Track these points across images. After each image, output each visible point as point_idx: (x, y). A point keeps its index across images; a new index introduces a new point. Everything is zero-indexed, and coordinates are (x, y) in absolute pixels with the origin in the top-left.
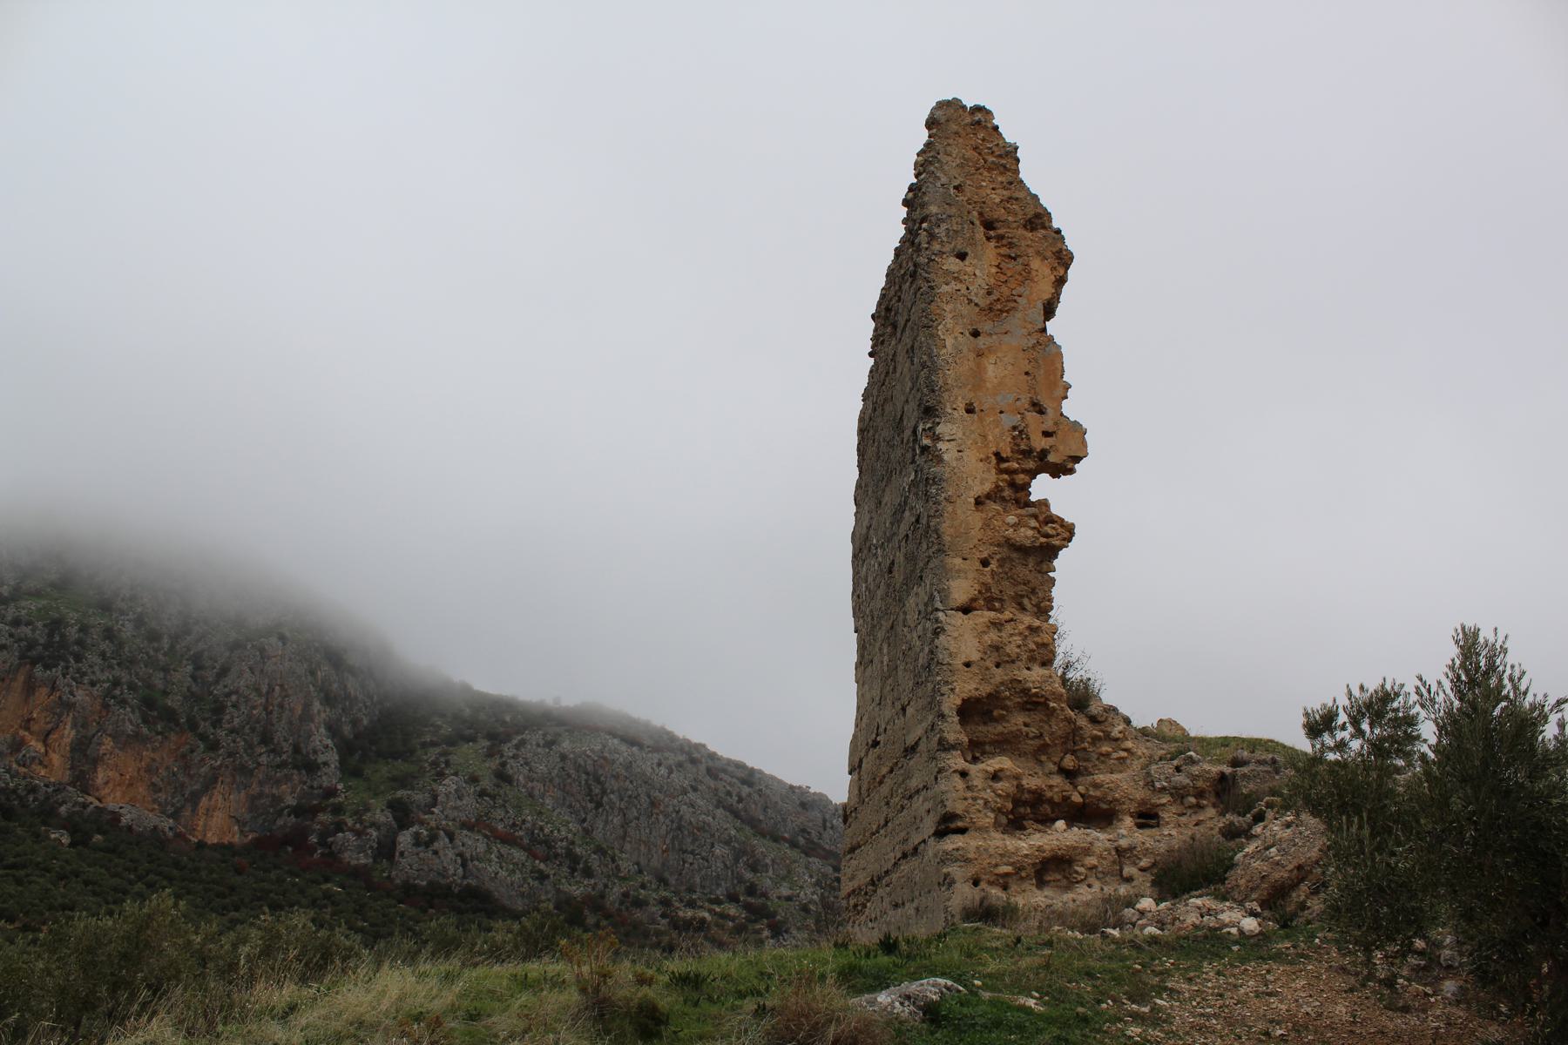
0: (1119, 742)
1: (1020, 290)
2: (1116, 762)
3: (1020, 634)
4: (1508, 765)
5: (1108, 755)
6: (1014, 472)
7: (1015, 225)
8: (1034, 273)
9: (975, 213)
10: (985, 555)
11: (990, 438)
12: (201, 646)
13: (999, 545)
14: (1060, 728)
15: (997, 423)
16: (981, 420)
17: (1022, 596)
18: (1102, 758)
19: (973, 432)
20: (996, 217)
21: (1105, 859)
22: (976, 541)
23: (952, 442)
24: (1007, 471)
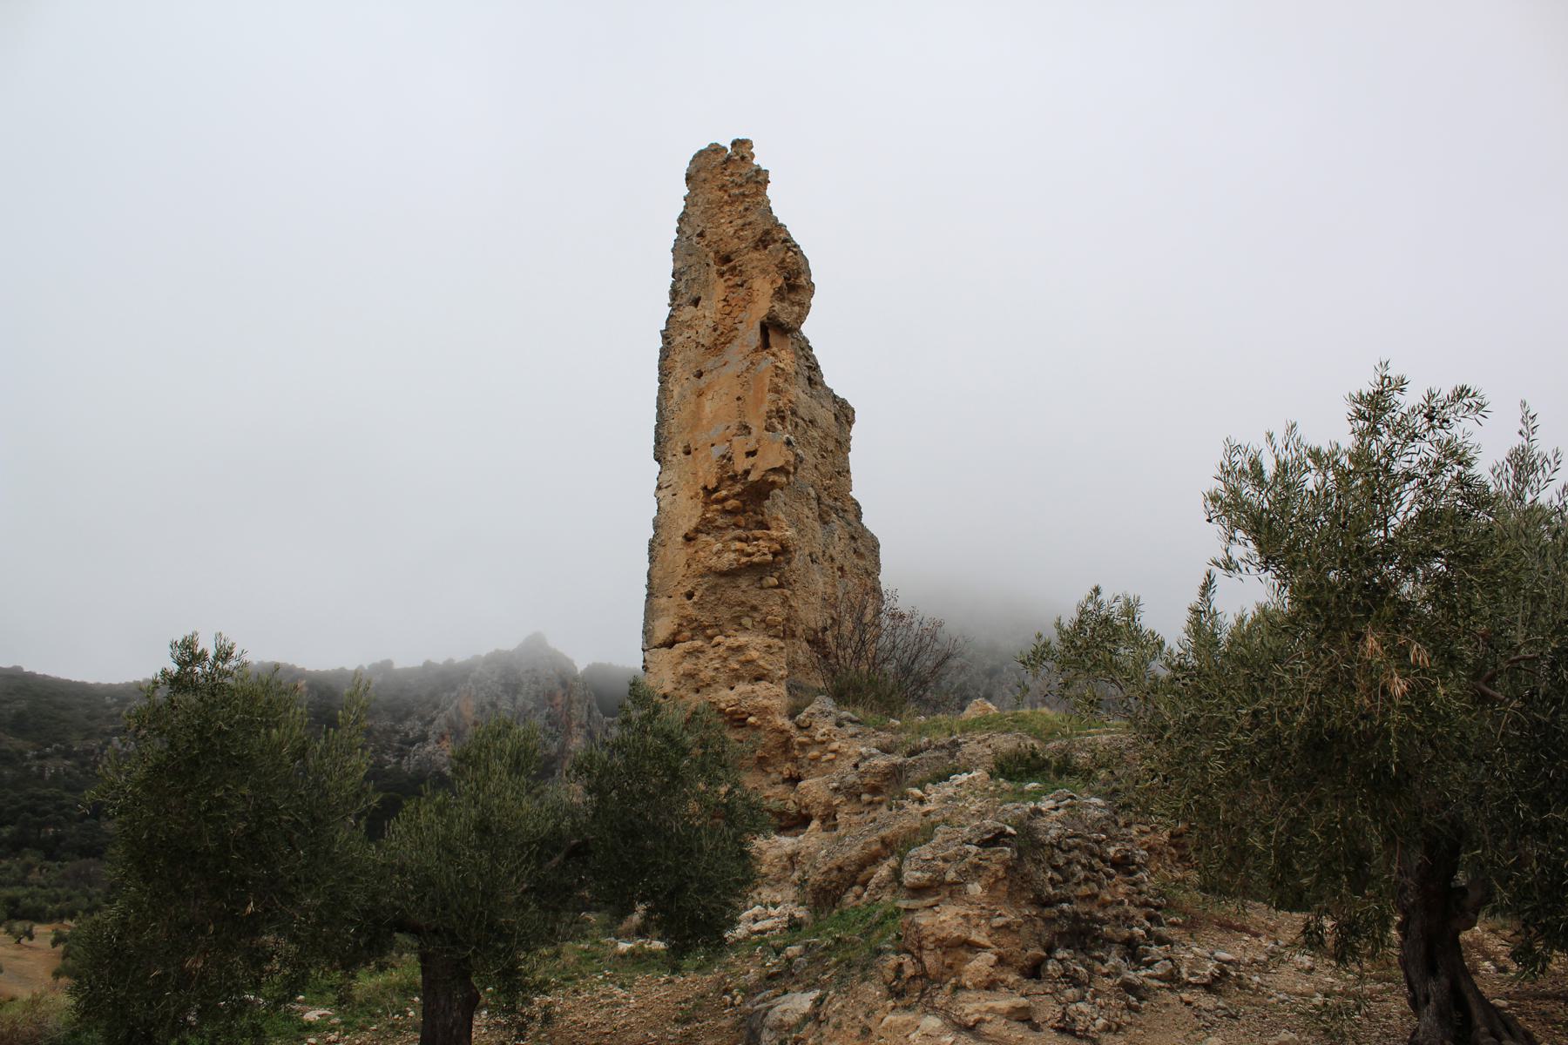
1: (742, 315)
2: (827, 765)
3: (720, 656)
4: (39, 833)
5: (816, 759)
6: (725, 499)
7: (745, 251)
8: (755, 294)
9: (712, 254)
10: (689, 588)
11: (701, 474)
12: (963, 678)
13: (702, 576)
14: (770, 740)
15: (708, 457)
16: (695, 458)
17: (739, 617)
18: (813, 763)
19: (686, 472)
20: (729, 250)
21: (776, 866)
22: (680, 578)
24: (717, 501)
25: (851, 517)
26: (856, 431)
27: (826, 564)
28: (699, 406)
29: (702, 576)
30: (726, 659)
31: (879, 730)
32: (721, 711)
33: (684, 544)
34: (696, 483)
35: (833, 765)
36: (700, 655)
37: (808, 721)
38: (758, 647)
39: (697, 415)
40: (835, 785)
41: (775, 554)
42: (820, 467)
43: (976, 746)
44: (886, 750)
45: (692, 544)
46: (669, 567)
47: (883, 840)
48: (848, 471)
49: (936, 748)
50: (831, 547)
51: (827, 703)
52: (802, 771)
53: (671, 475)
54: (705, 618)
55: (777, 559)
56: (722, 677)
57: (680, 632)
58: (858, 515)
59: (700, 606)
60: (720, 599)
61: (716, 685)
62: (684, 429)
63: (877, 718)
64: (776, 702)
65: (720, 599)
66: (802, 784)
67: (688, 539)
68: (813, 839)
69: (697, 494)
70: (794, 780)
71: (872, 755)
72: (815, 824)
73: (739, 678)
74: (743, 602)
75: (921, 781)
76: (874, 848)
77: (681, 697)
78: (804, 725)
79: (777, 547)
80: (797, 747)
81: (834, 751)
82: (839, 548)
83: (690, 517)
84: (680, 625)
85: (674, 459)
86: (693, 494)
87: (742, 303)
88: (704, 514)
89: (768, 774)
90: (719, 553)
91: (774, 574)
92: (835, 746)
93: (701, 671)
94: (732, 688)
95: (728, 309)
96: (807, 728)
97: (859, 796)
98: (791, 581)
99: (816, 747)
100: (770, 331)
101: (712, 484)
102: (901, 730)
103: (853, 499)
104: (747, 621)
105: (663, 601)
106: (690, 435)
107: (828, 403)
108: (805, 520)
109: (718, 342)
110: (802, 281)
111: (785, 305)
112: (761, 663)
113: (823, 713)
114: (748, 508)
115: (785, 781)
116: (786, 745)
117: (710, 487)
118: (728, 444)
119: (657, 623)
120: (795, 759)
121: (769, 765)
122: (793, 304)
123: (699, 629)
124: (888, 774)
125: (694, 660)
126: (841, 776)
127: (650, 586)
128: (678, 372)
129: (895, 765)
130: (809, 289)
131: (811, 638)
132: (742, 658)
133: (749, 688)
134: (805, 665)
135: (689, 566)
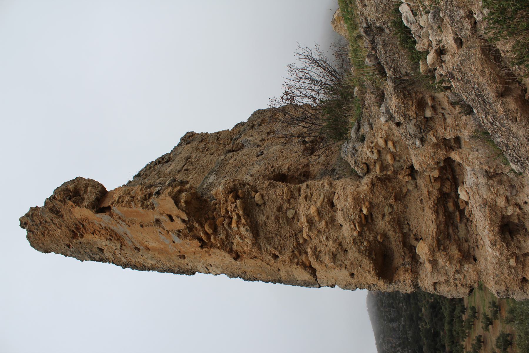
0: (381, 149)
5: (394, 156)
6: (206, 233)
8: (83, 217)
10: (270, 257)
13: (260, 248)
17: (288, 220)
18: (398, 159)
19: (195, 258)
20: (68, 232)
21: (498, 190)
22: (264, 263)
23: (207, 156)
24: (209, 237)
25: (242, 128)
26: (198, 131)
27: (265, 144)
28: (154, 249)
29: (260, 248)
30: (319, 231)
31: (364, 105)
32: (360, 234)
33: (242, 260)
34: (200, 252)
35: (398, 142)
36: (318, 249)
37: (361, 166)
38: (307, 207)
39: (161, 251)
40: (418, 143)
41: (237, 197)
42: (212, 152)
43: (368, 8)
44: (381, 98)
45: (240, 254)
46: (258, 270)
47: (501, 95)
48: (218, 133)
49: (374, 48)
50: (256, 141)
51: (347, 148)
52: (405, 167)
53: (200, 266)
54: (291, 244)
55: (241, 196)
56: (333, 233)
57: (303, 263)
58: (242, 124)
59: (282, 248)
60: (276, 234)
61: (340, 238)
62: (170, 258)
63: (354, 106)
64: (349, 191)
65: (276, 234)
66: (417, 167)
67: (237, 257)
68: (470, 157)
69: (206, 252)
70: (412, 172)
71: (387, 111)
72: (454, 156)
73: (333, 220)
74: (276, 218)
75: (413, 58)
76: (512, 105)
77: (352, 263)
78: (365, 169)
79: (230, 196)
80: (384, 173)
81: (386, 142)
82: (256, 137)
83: (221, 256)
84: (298, 264)
85: (190, 264)
86: (207, 255)
87: (91, 225)
88: (218, 248)
89: (408, 191)
90: (242, 238)
91: (253, 195)
92: (381, 142)
93: (330, 249)
94: (341, 225)
95: (97, 232)
96: (368, 166)
97: (427, 119)
98: (272, 170)
99: (384, 157)
100: (102, 206)
101: (196, 242)
102: (362, 86)
103: (233, 129)
104: (290, 214)
105: (282, 274)
106: (172, 255)
107: (180, 149)
108: (237, 161)
109: (116, 238)
110: (71, 187)
111: (86, 196)
112: (319, 204)
113: (354, 154)
114: (211, 216)
115: (414, 179)
116: (384, 180)
117: (200, 244)
118: (170, 233)
119: (299, 278)
120: (395, 173)
121: (401, 191)
122: (86, 192)
123: (300, 248)
124: (404, 94)
125: (322, 255)
126: (409, 137)
127: (275, 282)
128: (140, 260)
129: (395, 88)
130: (78, 181)
131: (310, 152)
132: (317, 219)
133: (340, 213)
134: (327, 156)
135: (255, 257)
